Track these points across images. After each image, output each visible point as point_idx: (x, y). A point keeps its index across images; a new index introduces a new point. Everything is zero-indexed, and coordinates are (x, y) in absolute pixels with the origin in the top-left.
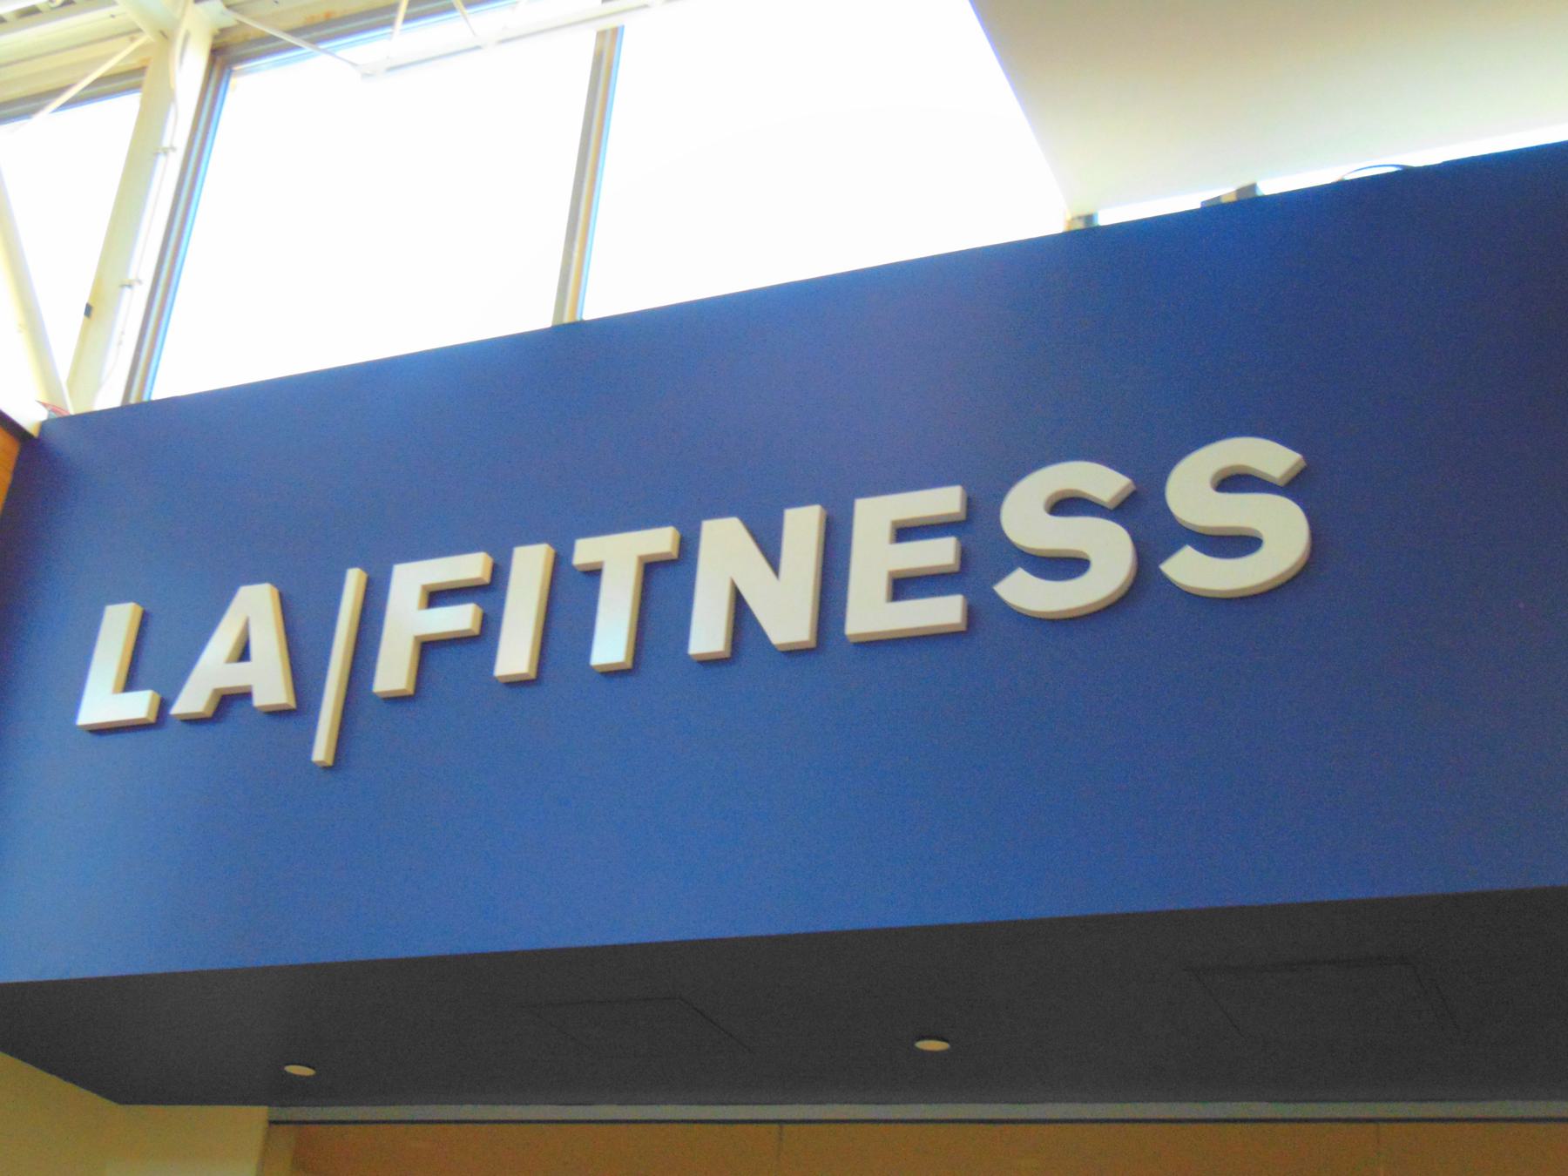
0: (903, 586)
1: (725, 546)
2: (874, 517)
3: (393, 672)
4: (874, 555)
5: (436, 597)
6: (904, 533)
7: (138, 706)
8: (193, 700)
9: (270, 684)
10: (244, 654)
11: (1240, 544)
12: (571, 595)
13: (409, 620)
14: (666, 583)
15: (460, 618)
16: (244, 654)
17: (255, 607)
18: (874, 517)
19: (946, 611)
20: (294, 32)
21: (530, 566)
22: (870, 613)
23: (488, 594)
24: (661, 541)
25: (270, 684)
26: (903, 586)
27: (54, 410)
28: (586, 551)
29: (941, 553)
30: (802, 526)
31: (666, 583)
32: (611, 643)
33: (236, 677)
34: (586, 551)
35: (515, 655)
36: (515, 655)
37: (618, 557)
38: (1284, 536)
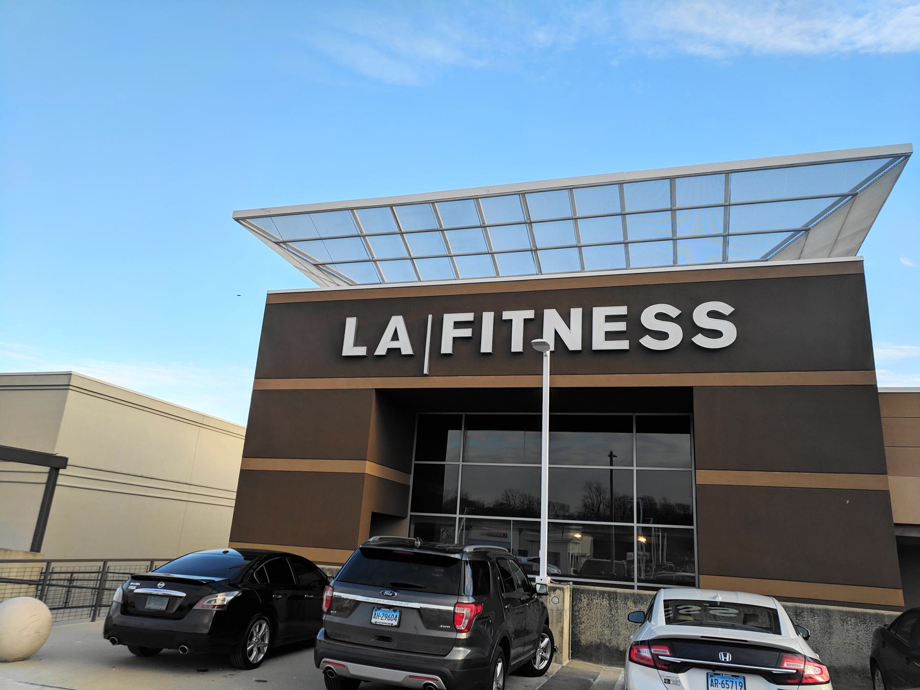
0: (610, 336)
1: (552, 319)
2: (599, 313)
3: (447, 347)
4: (600, 327)
5: (458, 325)
6: (609, 319)
7: (362, 351)
8: (381, 350)
9: (405, 346)
10: (395, 337)
11: (716, 334)
12: (503, 328)
13: (449, 333)
14: (534, 327)
15: (467, 332)
16: (395, 337)
17: (397, 322)
18: (599, 313)
19: (624, 345)
20: (554, 589)
21: (488, 318)
22: (599, 343)
23: (476, 325)
24: (530, 314)
25: (405, 346)
26: (610, 336)
27: (508, 499)
28: (506, 315)
29: (621, 326)
30: (576, 314)
31: (534, 327)
32: (517, 345)
33: (395, 345)
34: (506, 315)
35: (487, 346)
36: (487, 346)
37: (518, 318)
38: (729, 333)
